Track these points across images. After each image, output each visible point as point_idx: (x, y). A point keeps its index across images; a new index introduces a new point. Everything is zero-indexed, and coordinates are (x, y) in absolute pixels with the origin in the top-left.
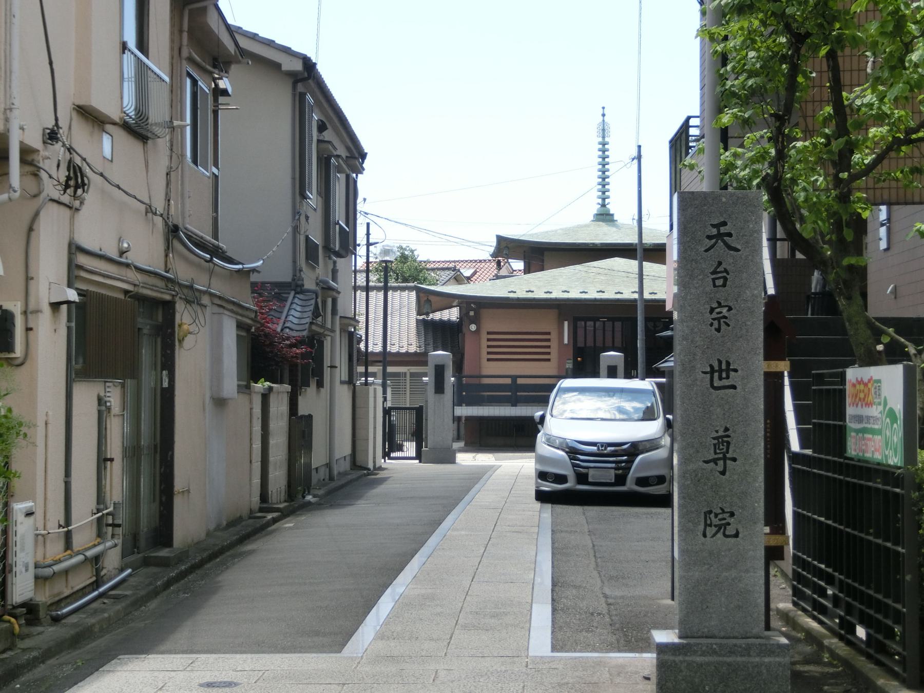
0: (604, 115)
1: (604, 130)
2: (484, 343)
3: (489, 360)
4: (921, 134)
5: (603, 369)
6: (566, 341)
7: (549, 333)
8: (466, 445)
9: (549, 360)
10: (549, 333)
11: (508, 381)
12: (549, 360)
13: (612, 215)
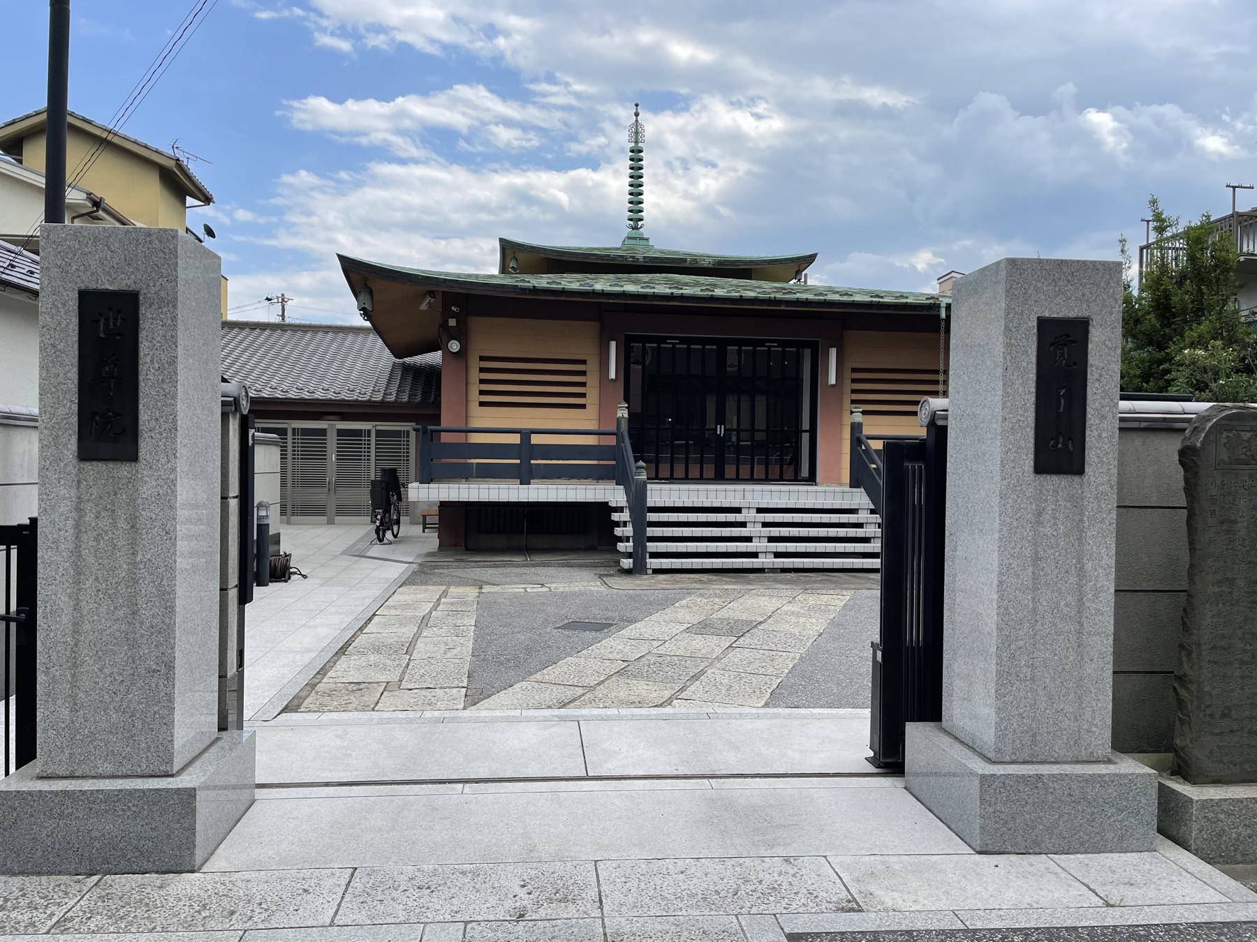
0: (637, 115)
1: (637, 133)
2: (475, 376)
3: (482, 404)
5: (1181, 378)
6: (612, 375)
7: (584, 362)
8: (441, 546)
10: (584, 362)
11: (515, 439)
12: (583, 406)
13: (647, 239)
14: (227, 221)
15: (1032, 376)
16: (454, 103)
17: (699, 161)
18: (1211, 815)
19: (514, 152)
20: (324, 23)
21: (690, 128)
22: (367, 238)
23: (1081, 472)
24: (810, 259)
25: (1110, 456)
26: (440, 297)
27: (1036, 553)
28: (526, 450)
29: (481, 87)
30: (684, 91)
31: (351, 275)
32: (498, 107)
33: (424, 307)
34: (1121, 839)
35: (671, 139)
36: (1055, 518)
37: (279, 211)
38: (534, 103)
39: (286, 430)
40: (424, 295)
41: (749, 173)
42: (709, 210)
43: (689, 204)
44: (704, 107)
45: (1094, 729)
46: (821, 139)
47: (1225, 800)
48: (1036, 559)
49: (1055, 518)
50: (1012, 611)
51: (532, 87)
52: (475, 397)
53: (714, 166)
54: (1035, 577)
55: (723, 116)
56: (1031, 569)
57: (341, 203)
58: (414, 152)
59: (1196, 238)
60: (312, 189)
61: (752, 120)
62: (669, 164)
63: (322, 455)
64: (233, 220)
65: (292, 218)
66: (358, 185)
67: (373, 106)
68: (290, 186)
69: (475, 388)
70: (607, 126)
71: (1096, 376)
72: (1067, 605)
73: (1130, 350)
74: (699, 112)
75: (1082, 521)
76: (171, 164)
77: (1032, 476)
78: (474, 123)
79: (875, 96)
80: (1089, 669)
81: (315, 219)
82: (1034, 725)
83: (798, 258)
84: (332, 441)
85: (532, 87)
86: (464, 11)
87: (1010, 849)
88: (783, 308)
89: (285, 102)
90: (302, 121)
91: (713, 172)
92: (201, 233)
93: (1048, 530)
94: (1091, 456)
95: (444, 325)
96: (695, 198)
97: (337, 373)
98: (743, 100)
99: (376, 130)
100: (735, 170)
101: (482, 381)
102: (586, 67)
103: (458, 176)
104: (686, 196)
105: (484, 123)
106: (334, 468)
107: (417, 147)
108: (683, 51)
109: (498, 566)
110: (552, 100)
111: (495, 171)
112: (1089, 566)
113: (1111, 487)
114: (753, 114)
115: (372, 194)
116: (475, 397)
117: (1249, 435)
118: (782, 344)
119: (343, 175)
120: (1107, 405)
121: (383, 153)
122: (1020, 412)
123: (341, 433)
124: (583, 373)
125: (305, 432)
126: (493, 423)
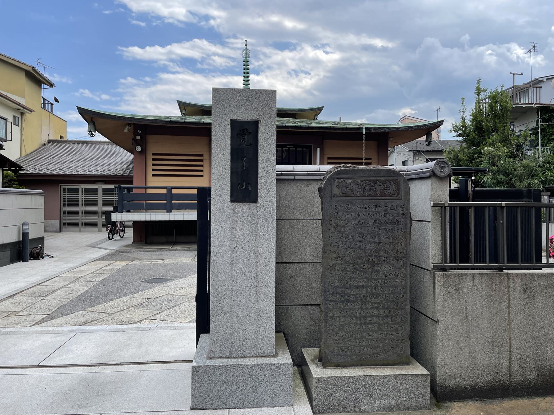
2: (150, 162)
3: (153, 175)
4: (553, 137)
7: (202, 155)
9: (202, 176)
10: (202, 155)
11: (164, 191)
12: (202, 176)
14: (98, 99)
15: (228, 151)
16: (193, 47)
17: (303, 72)
18: (323, 386)
19: (221, 68)
20: (133, 15)
21: (297, 57)
22: (160, 106)
23: (255, 201)
24: (321, 109)
25: (272, 193)
26: (132, 126)
27: (232, 244)
28: (169, 196)
29: (204, 40)
30: (294, 41)
31: (85, 116)
32: (213, 48)
33: (126, 131)
34: (272, 399)
35: (289, 62)
36: (242, 226)
37: (121, 95)
38: (228, 47)
39: (79, 189)
40: (126, 126)
41: (325, 76)
42: (309, 92)
43: (299, 90)
44: (302, 49)
45: (265, 338)
46: (355, 62)
47: (332, 377)
48: (232, 248)
49: (242, 226)
50: (220, 276)
51: (227, 40)
52: (150, 172)
53: (310, 74)
54: (232, 257)
55: (311, 53)
56: (229, 253)
57: (148, 91)
58: (178, 69)
59: (494, 97)
60: (134, 85)
61: (324, 54)
62: (289, 73)
63: (96, 200)
64: (101, 99)
65: (127, 98)
66: (154, 84)
67: (158, 49)
68: (124, 84)
69: (150, 168)
70: (262, 57)
71: (263, 151)
72: (249, 272)
73: (465, 148)
74: (301, 50)
75: (257, 227)
76: (30, 69)
77: (230, 204)
78: (205, 56)
79: (378, 43)
80: (262, 306)
81: (136, 98)
82: (232, 337)
83: (315, 109)
84: (100, 194)
85: (227, 40)
86: (194, 8)
87: (209, 407)
88: (290, 130)
89: (119, 48)
90: (128, 57)
91: (309, 77)
92: (53, 101)
93: (239, 232)
94: (261, 192)
95: (134, 139)
96: (301, 87)
97: (105, 163)
98: (319, 45)
99: (161, 60)
100: (319, 75)
101: (153, 165)
102: (249, 31)
103: (198, 78)
104: (297, 86)
105: (209, 56)
106: (101, 206)
107: (179, 67)
108: (289, 24)
109: (150, 251)
110: (235, 46)
111: (214, 77)
112: (261, 251)
113: (273, 209)
114: (324, 52)
115: (160, 87)
116: (150, 172)
117: (350, 181)
118: (294, 146)
119: (148, 79)
120: (269, 167)
121: (165, 69)
122: (222, 169)
123: (104, 190)
124: (202, 161)
125: (87, 190)
126: (157, 184)
